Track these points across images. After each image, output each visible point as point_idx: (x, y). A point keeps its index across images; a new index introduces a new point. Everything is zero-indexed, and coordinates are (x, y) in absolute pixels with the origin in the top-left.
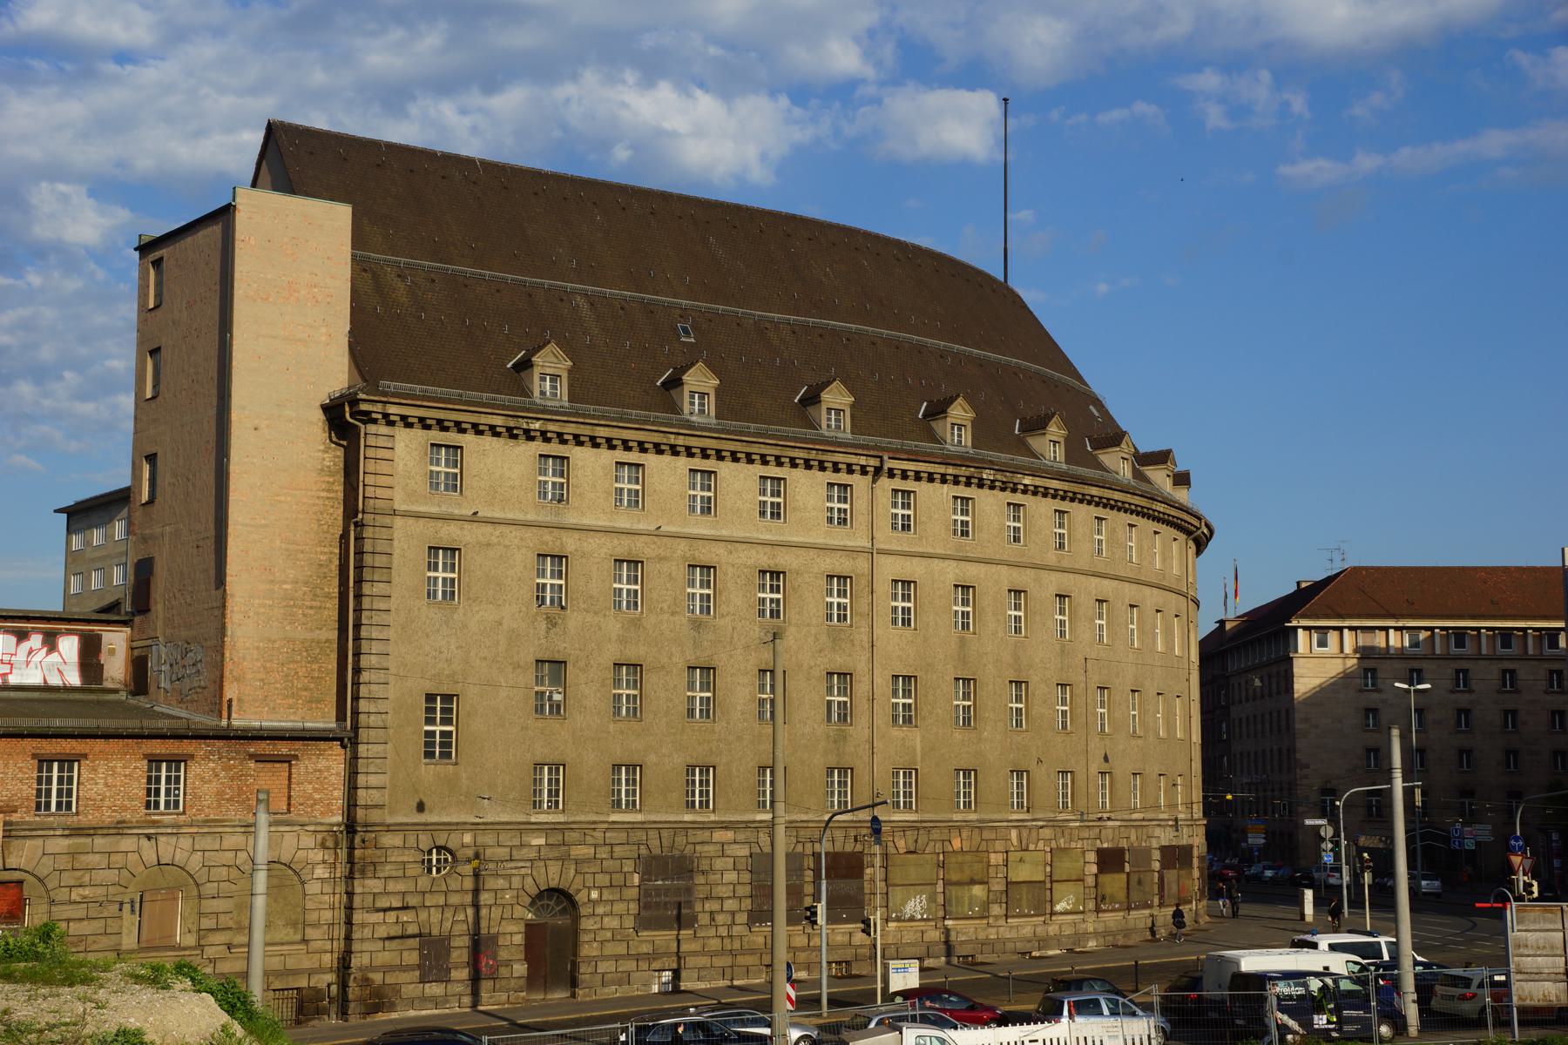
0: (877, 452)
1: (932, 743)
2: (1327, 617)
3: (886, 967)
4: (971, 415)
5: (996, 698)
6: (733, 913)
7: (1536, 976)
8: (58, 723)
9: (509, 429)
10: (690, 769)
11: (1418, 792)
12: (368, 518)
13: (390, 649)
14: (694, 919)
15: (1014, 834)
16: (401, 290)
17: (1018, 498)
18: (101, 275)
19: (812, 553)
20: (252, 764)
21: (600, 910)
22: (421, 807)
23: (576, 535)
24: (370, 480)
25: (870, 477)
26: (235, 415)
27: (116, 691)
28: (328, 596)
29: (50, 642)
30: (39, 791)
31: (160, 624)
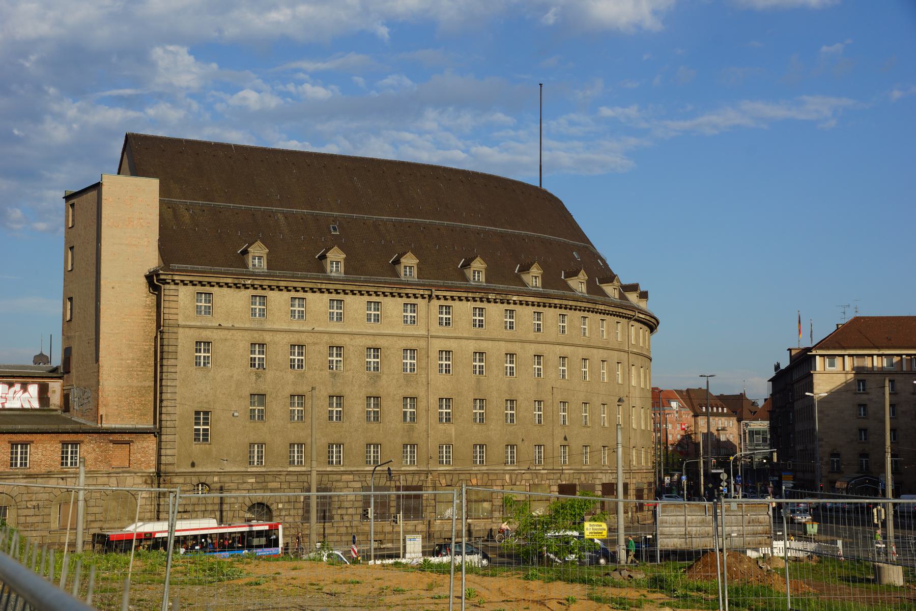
0: (428, 287)
1: (462, 431)
2: (835, 348)
3: (404, 540)
4: (485, 266)
5: (497, 408)
6: (352, 515)
7: (670, 536)
8: (19, 427)
9: (235, 284)
10: (330, 446)
11: (775, 455)
12: (166, 329)
13: (177, 391)
14: (331, 518)
15: (507, 477)
16: (186, 217)
17: (511, 307)
18: (195, 106)
19: (395, 338)
20: (111, 445)
21: (283, 513)
22: (193, 465)
23: (271, 334)
24: (166, 311)
25: (427, 300)
26: (103, 282)
27: (56, 410)
28: (149, 365)
29: (24, 387)
30: (12, 458)
31: (74, 378)
